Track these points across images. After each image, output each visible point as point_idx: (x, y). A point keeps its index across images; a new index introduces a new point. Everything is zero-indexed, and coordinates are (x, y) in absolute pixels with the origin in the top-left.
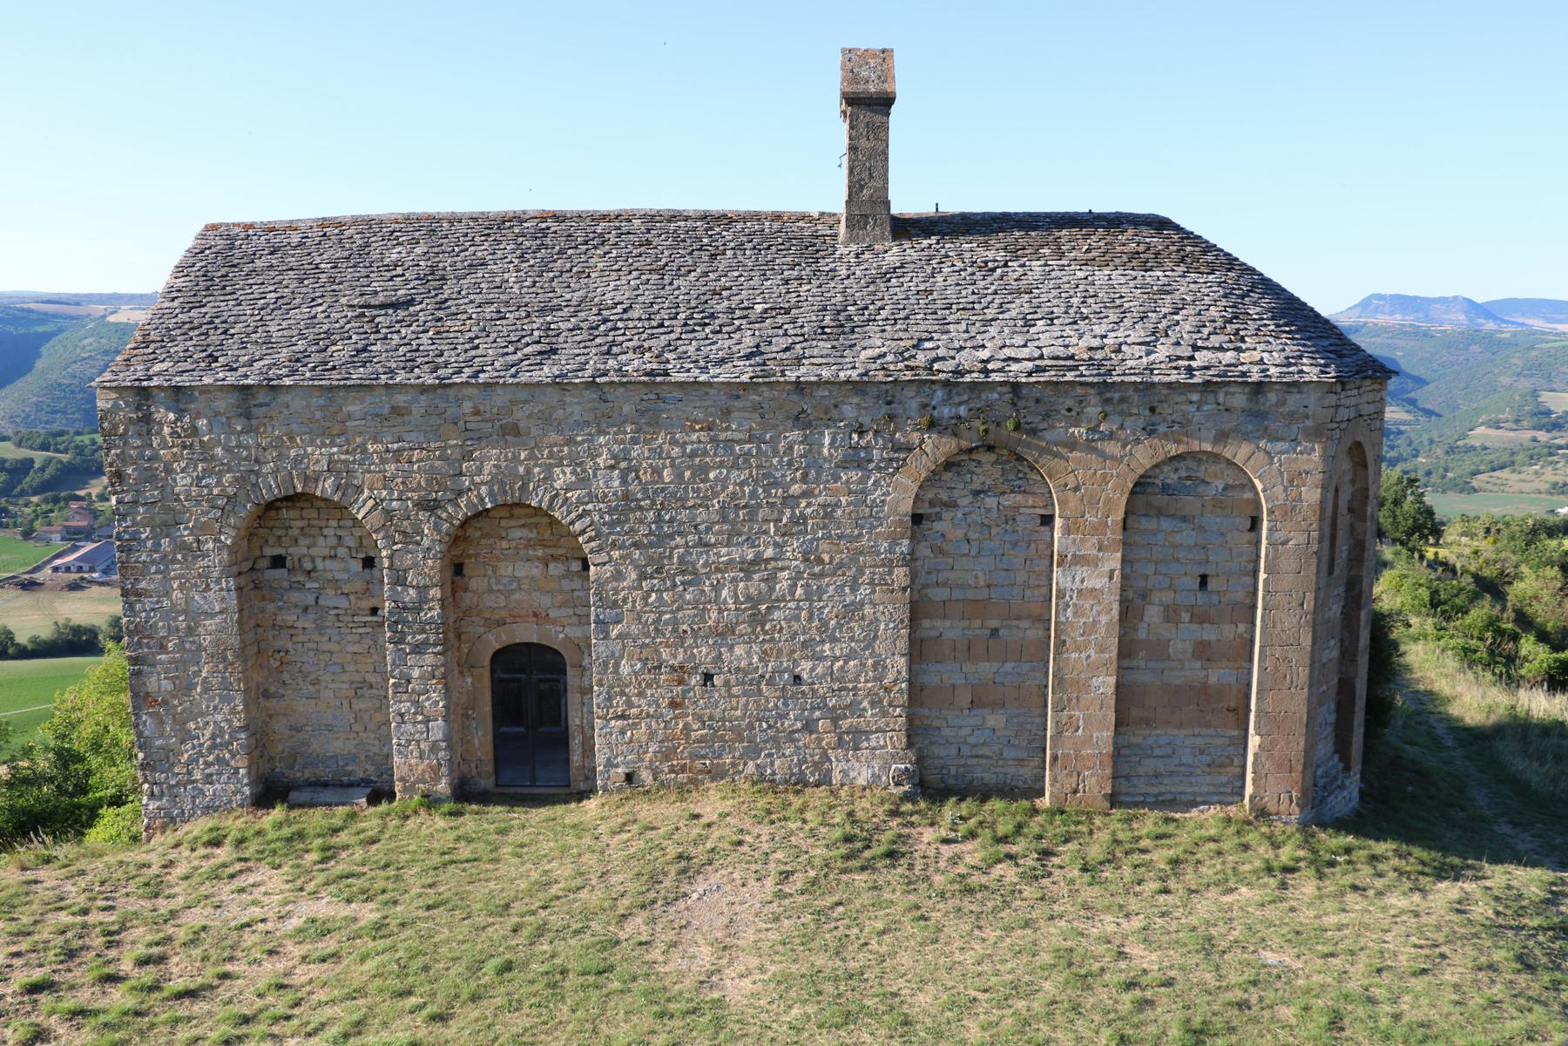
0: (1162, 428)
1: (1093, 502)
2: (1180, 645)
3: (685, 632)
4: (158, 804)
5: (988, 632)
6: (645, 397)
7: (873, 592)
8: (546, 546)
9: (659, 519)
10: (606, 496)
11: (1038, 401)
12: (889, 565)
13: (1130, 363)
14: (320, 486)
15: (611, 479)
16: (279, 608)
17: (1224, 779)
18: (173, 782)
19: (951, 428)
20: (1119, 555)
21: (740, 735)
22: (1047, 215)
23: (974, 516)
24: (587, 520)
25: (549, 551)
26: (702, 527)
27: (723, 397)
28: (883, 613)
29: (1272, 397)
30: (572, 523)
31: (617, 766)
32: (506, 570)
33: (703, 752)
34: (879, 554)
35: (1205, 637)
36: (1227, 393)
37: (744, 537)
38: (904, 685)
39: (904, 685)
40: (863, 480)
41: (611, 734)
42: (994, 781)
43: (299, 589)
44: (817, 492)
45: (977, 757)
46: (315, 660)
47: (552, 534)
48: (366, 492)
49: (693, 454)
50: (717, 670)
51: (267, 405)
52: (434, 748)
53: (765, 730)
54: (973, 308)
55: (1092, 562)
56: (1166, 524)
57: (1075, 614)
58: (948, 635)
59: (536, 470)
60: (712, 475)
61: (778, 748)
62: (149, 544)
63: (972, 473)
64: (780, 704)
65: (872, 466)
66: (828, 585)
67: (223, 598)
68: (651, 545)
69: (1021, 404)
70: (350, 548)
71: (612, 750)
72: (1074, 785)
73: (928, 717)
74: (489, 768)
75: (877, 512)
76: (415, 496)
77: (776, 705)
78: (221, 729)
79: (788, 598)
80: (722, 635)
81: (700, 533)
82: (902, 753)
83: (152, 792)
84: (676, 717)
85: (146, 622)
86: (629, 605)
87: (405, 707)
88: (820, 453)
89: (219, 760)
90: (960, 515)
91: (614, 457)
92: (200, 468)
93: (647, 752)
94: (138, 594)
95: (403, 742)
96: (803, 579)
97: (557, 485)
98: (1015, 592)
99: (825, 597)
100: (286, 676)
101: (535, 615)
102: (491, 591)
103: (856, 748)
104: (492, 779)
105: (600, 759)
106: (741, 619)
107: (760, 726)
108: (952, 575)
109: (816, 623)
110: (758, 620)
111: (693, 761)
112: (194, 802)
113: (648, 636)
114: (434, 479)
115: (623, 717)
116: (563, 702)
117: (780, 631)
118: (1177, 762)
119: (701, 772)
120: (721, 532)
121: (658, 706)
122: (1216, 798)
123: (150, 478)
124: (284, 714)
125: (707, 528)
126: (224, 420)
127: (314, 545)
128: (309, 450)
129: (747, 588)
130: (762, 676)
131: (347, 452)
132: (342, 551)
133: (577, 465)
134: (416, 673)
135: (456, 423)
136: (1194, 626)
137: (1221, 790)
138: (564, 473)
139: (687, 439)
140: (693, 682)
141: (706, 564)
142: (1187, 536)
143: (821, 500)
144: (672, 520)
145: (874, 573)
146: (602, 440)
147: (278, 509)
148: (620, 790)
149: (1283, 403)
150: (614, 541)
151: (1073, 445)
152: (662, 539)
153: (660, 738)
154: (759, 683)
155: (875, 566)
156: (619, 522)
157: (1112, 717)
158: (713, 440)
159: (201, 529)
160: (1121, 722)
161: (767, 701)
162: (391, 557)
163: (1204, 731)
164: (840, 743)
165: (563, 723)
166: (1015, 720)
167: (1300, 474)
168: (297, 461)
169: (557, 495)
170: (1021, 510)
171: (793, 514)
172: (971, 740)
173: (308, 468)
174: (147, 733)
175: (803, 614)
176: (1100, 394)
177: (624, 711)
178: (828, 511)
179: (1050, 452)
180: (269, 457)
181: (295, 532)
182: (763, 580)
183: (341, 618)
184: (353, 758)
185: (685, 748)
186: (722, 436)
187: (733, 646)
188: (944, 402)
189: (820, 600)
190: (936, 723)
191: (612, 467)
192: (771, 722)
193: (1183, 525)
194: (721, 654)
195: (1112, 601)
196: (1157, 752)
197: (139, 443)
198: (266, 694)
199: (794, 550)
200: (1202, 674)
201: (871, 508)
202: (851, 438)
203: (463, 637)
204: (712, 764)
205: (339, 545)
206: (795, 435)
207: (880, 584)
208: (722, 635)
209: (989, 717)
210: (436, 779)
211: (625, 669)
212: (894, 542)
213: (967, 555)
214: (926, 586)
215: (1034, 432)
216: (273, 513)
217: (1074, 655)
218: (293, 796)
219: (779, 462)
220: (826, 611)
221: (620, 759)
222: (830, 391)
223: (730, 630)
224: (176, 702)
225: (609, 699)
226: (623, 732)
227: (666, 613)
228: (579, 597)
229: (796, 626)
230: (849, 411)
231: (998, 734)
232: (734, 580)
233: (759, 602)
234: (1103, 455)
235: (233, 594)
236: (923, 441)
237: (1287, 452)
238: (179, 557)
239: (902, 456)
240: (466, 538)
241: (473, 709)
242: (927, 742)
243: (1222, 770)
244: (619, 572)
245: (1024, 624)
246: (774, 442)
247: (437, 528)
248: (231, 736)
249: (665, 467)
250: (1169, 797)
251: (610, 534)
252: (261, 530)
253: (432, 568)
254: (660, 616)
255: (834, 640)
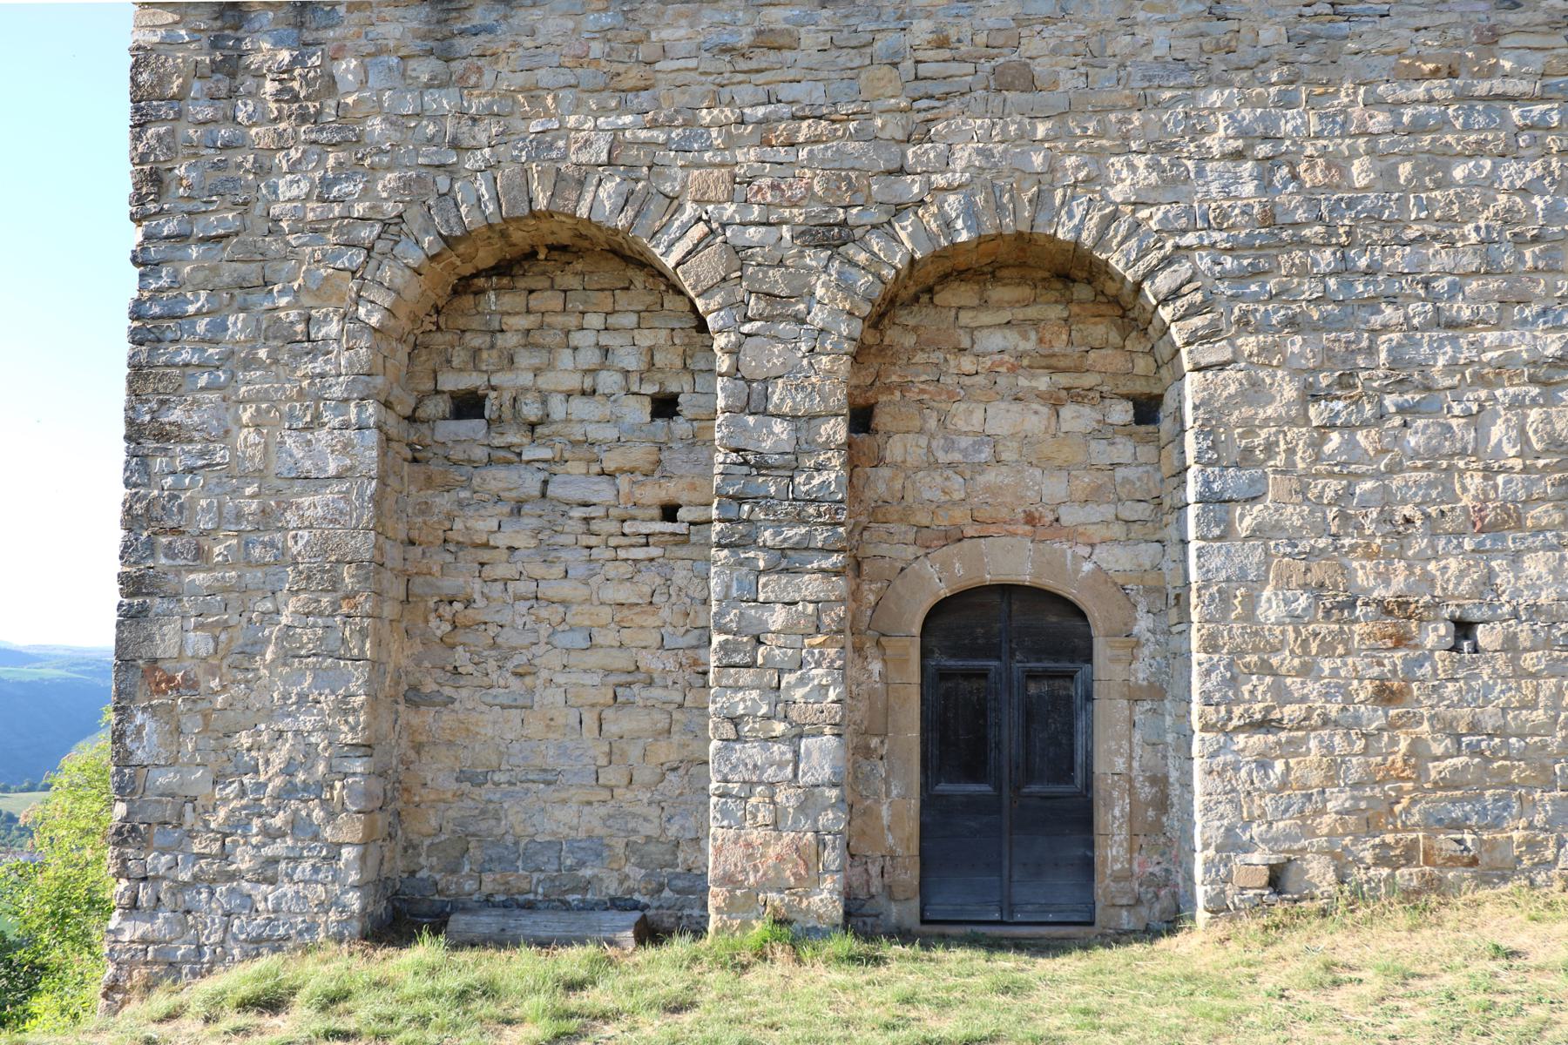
3: (1408, 521)
4: (143, 928)
8: (1055, 370)
9: (1344, 269)
14: (588, 197)
15: (1237, 179)
16: (461, 504)
18: (185, 876)
24: (1184, 269)
25: (1063, 380)
26: (1441, 285)
30: (1151, 274)
31: (1248, 848)
32: (968, 417)
33: (1457, 813)
37: (1536, 308)
41: (1237, 769)
43: (509, 463)
46: (529, 619)
47: (1070, 342)
48: (690, 210)
49: (1417, 128)
50: (1486, 612)
51: (489, 30)
52: (809, 802)
59: (1071, 161)
60: (1459, 173)
62: (202, 326)
67: (347, 446)
68: (1327, 324)
70: (626, 373)
71: (1238, 807)
74: (909, 875)
76: (798, 215)
78: (310, 752)
80: (1494, 528)
81: (1436, 299)
83: (135, 899)
84: (1392, 726)
85: (173, 497)
86: (1280, 461)
87: (741, 703)
89: (296, 825)
91: (1243, 133)
92: (331, 162)
93: (1319, 812)
94: (162, 435)
95: (735, 788)
97: (1117, 194)
100: (461, 656)
101: (1030, 519)
102: (933, 465)
104: (915, 904)
105: (1204, 830)
111: (1431, 835)
112: (227, 928)
113: (1324, 531)
114: (842, 178)
115: (1265, 725)
116: (1080, 725)
119: (1452, 861)
120: (1483, 297)
121: (1348, 698)
123: (222, 187)
124: (450, 744)
125: (1452, 285)
126: (394, 61)
127: (550, 366)
128: (572, 121)
129: (1547, 420)
131: (654, 125)
132: (609, 381)
133: (1162, 150)
134: (777, 618)
135: (895, 65)
138: (1132, 168)
140: (1430, 640)
141: (1452, 367)
144: (1370, 272)
146: (1215, 97)
147: (481, 292)
148: (1258, 906)
150: (1245, 313)
152: (1353, 310)
153: (1354, 776)
156: (1256, 273)
159: (316, 294)
162: (734, 351)
165: (1079, 774)
168: (542, 143)
169: (1114, 216)
173: (565, 157)
174: (140, 755)
177: (1268, 710)
180: (483, 138)
181: (510, 340)
183: (595, 526)
184: (597, 849)
185: (1414, 802)
186: (1482, 88)
191: (1238, 156)
194: (1490, 575)
197: (208, 113)
198: (414, 697)
203: (866, 568)
205: (603, 367)
208: (1494, 528)
210: (809, 880)
211: (1270, 608)
216: (467, 301)
218: (458, 922)
221: (1256, 830)
224: (215, 684)
226: (1264, 764)
227: (1363, 476)
228: (1126, 480)
232: (1517, 403)
235: (372, 436)
238: (262, 353)
240: (882, 349)
241: (884, 735)
244: (1255, 384)
247: (846, 287)
248: (330, 768)
249: (1354, 154)
251: (1234, 297)
252: (438, 337)
253: (830, 373)
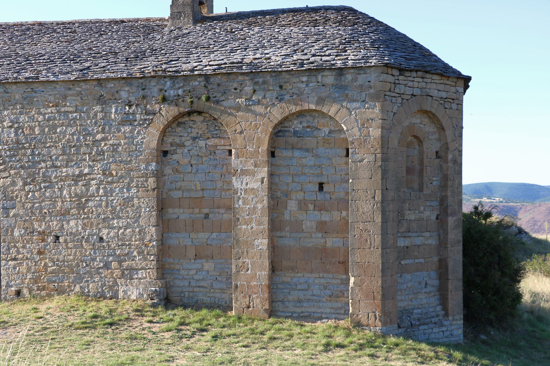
0: (287, 97)
1: (251, 140)
2: (308, 224)
3: (46, 213)
5: (203, 216)
6: (26, 90)
7: (138, 191)
9: (33, 154)
10: (8, 142)
11: (219, 85)
12: (146, 176)
13: (272, 63)
17: (339, 305)
19: (176, 101)
20: (266, 169)
21: (72, 269)
22: (278, 10)
23: (193, 151)
26: (54, 157)
27: (63, 89)
28: (143, 203)
29: (349, 77)
31: (12, 286)
33: (54, 279)
34: (140, 171)
35: (323, 219)
36: (323, 76)
37: (74, 163)
38: (154, 243)
39: (154, 243)
40: (132, 131)
41: (9, 269)
42: (209, 302)
44: (109, 138)
45: (199, 287)
49: (49, 120)
50: (61, 234)
53: (85, 267)
54: (209, 47)
55: (252, 174)
56: (297, 153)
57: (244, 203)
58: (182, 217)
60: (58, 130)
61: (92, 278)
63: (191, 127)
64: (92, 253)
65: (136, 123)
66: (115, 188)
68: (29, 167)
69: (210, 87)
71: (9, 278)
72: (247, 303)
73: (173, 264)
75: (139, 148)
77: (90, 253)
79: (96, 195)
81: (53, 161)
82: (154, 281)
86: (19, 199)
88: (110, 117)
90: (186, 151)
91: (11, 121)
93: (26, 279)
96: (103, 184)
98: (216, 193)
99: (114, 194)
103: (131, 279)
106: (72, 206)
107: (82, 265)
108: (183, 184)
109: (110, 208)
110: (81, 207)
111: (49, 284)
113: (28, 216)
115: (15, 259)
117: (92, 213)
118: (310, 293)
121: (32, 253)
122: (334, 316)
129: (75, 189)
130: (83, 237)
136: (316, 213)
137: (338, 312)
139: (46, 111)
140: (49, 240)
141: (56, 177)
142: (310, 161)
143: (111, 142)
144: (39, 154)
145: (138, 181)
146: (6, 113)
149: (356, 80)
150: (11, 165)
151: (238, 108)
152: (35, 164)
153: (33, 271)
154: (81, 242)
155: (139, 177)
156: (14, 156)
157: (267, 263)
158: (59, 112)
160: (273, 269)
161: (86, 251)
163: (326, 275)
164: (123, 276)
166: (219, 266)
167: (368, 120)
170: (218, 148)
171: (98, 150)
172: (196, 277)
175: (103, 203)
176: (252, 79)
177: (15, 256)
178: (114, 148)
179: (226, 112)
182: (83, 185)
185: (45, 277)
186: (63, 109)
187: (69, 220)
188: (171, 88)
189: (112, 196)
190: (177, 267)
191: (11, 127)
192: (88, 263)
193: (307, 154)
194: (63, 225)
195: (264, 194)
196: (299, 287)
199: (98, 169)
200: (323, 241)
201: (136, 146)
202: (125, 109)
204: (58, 285)
206: (98, 108)
207: (142, 187)
209: (205, 264)
211: (16, 233)
212: (148, 164)
213: (191, 173)
214: (170, 190)
215: (217, 102)
217: (244, 227)
219: (91, 122)
220: (115, 202)
222: (114, 84)
223: (67, 212)
225: (9, 249)
226: (15, 268)
227: (36, 203)
229: (100, 210)
230: (124, 95)
231: (210, 274)
233: (82, 197)
234: (256, 114)
236: (160, 109)
237: (360, 108)
239: (151, 117)
242: (173, 278)
243: (338, 299)
244: (14, 182)
245: (222, 211)
246: (87, 112)
249: (36, 126)
250: (306, 314)
254: (34, 205)
255: (119, 218)
